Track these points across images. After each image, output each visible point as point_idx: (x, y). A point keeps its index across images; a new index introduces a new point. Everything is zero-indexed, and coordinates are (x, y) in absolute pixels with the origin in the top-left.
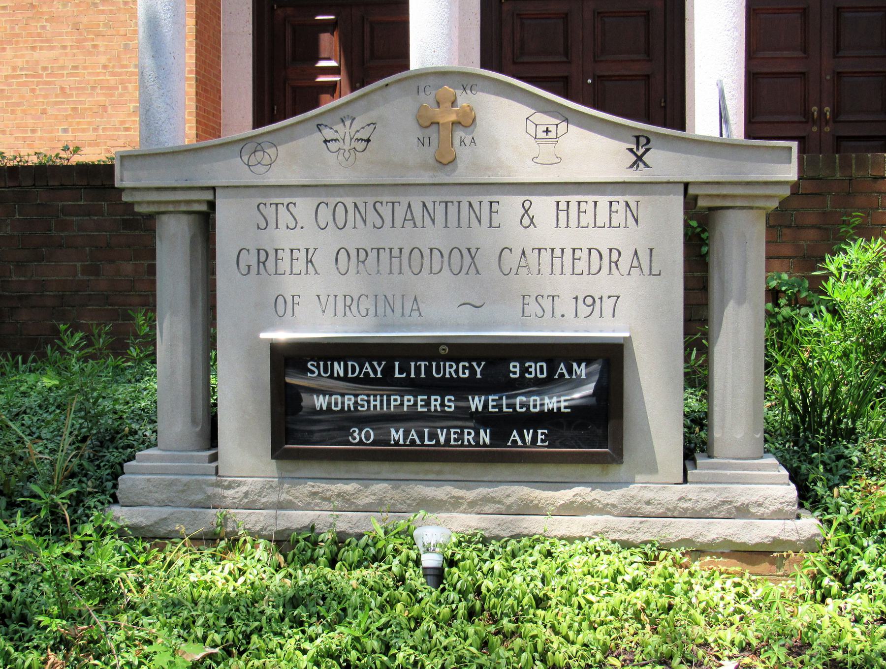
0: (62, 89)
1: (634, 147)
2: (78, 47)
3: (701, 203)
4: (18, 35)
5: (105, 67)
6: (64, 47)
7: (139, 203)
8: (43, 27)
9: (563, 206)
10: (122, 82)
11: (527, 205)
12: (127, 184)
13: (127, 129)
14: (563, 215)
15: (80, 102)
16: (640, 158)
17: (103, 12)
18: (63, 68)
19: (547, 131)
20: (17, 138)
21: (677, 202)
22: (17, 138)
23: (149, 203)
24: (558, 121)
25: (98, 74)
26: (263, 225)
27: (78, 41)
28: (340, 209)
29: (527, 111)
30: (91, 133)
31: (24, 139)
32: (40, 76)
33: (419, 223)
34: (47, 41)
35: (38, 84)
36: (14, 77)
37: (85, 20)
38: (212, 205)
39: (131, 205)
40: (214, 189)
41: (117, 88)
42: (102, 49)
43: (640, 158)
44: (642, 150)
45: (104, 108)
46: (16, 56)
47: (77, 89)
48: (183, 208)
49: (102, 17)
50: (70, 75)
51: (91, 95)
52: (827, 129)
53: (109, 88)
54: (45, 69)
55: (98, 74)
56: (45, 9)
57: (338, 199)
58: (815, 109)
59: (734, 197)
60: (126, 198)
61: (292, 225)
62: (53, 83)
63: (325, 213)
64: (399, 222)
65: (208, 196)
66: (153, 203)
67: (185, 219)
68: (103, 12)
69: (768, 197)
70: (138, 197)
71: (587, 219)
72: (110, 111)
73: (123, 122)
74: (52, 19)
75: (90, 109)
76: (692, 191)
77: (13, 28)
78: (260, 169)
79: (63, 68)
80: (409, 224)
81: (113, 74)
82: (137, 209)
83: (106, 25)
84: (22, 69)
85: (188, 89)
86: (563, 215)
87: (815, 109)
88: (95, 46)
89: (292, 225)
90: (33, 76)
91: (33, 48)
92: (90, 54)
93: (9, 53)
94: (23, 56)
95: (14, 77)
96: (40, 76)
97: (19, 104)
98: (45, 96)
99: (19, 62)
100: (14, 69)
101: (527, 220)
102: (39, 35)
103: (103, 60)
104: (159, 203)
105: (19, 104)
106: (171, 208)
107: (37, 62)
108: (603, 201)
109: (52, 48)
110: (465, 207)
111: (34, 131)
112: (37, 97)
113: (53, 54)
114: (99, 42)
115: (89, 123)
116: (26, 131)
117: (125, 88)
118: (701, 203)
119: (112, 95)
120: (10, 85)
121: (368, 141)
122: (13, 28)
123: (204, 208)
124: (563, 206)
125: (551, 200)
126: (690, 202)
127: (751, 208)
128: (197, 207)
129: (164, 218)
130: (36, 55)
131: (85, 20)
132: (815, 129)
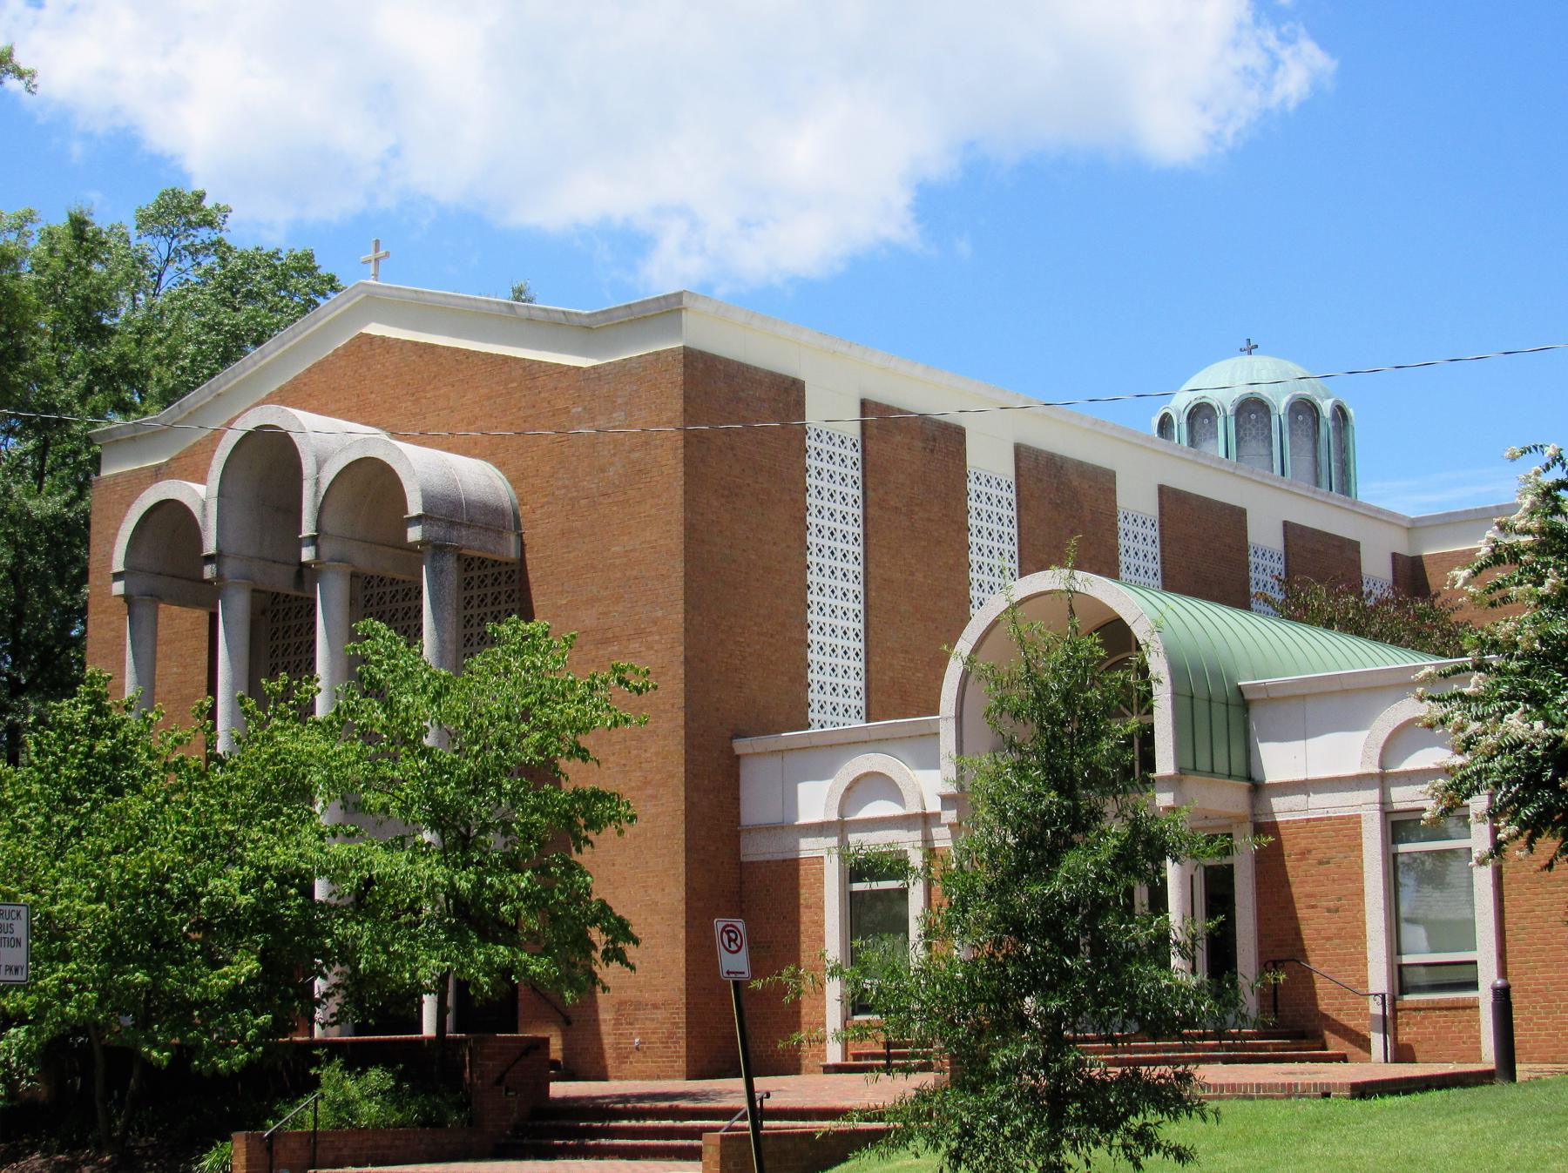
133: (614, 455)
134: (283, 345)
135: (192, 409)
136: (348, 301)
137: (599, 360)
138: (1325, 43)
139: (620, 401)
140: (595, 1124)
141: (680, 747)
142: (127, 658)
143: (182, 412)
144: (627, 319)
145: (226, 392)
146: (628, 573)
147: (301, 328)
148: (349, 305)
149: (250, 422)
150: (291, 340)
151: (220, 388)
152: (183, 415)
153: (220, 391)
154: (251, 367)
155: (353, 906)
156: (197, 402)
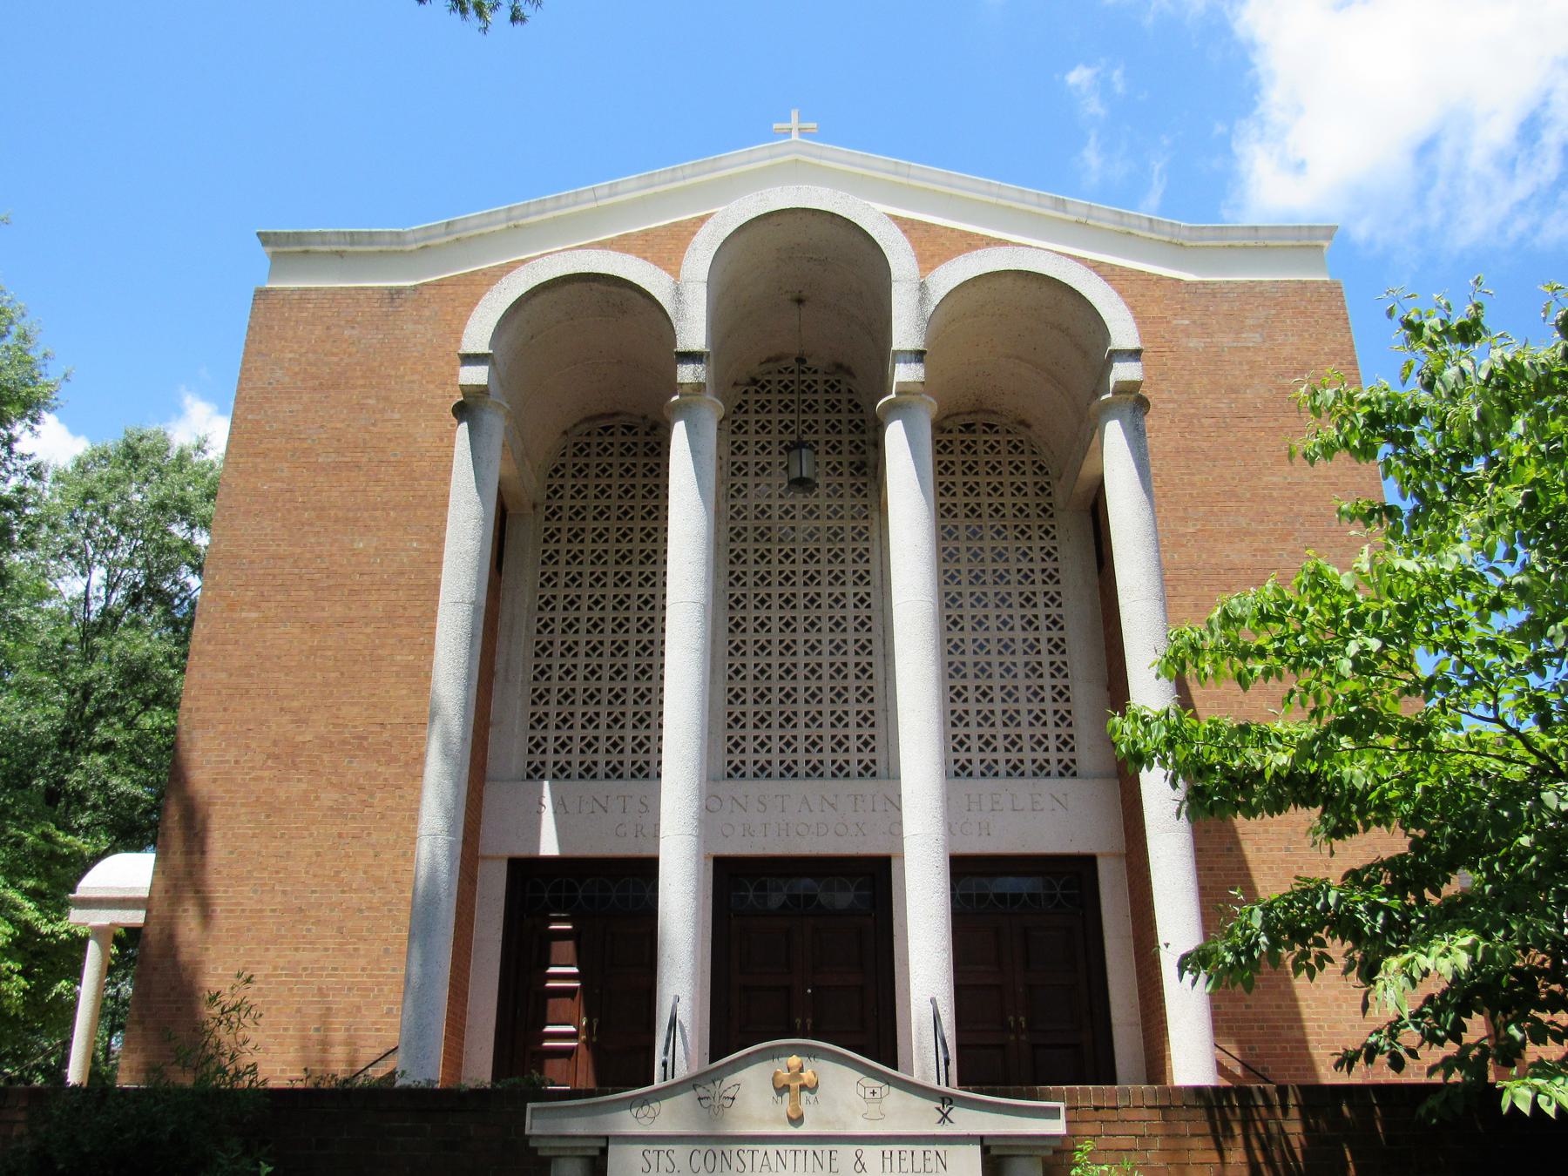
0: (320, 989)
1: (940, 1105)
2: (340, 950)
3: (994, 1152)
4: (283, 936)
5: (363, 969)
6: (326, 949)
7: (542, 1148)
8: (309, 930)
9: (887, 1155)
10: (379, 984)
11: (859, 1153)
12: (535, 1132)
13: (378, 1030)
14: (887, 1162)
15: (335, 1003)
16: (945, 1116)
17: (367, 918)
18: (322, 969)
19: (874, 1093)
20: (268, 1036)
21: (976, 1150)
22: (268, 1036)
23: (551, 1148)
24: (882, 1084)
25: (356, 976)
26: (647, 1169)
27: (341, 944)
28: (711, 1155)
29: (858, 1075)
30: (342, 1033)
31: (276, 1037)
32: (300, 976)
33: (774, 1168)
34: (310, 943)
35: (297, 982)
36: (273, 976)
37: (350, 924)
38: (604, 1152)
39: (536, 1149)
40: (607, 1138)
41: (373, 990)
42: (362, 952)
43: (945, 1116)
44: (947, 1109)
45: (359, 1008)
46: (279, 956)
47: (334, 989)
48: (579, 1153)
49: (366, 923)
50: (329, 976)
51: (347, 996)
52: (1023, 1037)
53: (366, 989)
54: (305, 969)
55: (356, 976)
56: (313, 913)
57: (709, 1147)
58: (1011, 1018)
59: (1018, 1147)
60: (532, 1144)
61: (670, 1169)
62: (312, 983)
63: (699, 1159)
64: (757, 1167)
65: (603, 1144)
66: (555, 1148)
67: (578, 1162)
68: (367, 918)
69: (1043, 1148)
70: (543, 1143)
71: (906, 1165)
72: (363, 1012)
73: (375, 1023)
74: (318, 922)
75: (345, 1009)
76: (987, 1142)
77: (279, 930)
78: (646, 1121)
79: (322, 969)
80: (765, 1169)
81: (370, 976)
82: (540, 1153)
83: (369, 930)
84: (282, 969)
85: (444, 993)
86: (887, 1162)
87: (1011, 1018)
88: (356, 950)
89: (670, 1169)
90: (294, 976)
91: (296, 949)
92: (351, 956)
93: (272, 954)
94: (285, 956)
95: (273, 976)
96: (300, 976)
97: (275, 1003)
98: (303, 996)
99: (281, 962)
100: (275, 968)
101: (859, 1167)
102: (304, 937)
103: (362, 962)
104: (560, 1148)
105: (275, 1003)
106: (569, 1153)
107: (299, 963)
108: (919, 1149)
109: (314, 950)
110: (810, 1154)
111: (286, 1030)
112: (294, 995)
113: (315, 955)
114: (361, 946)
115: (342, 1023)
116: (279, 1030)
117: (381, 990)
118: (994, 1152)
119: (368, 996)
120: (270, 983)
121: (733, 1099)
122: (279, 930)
123: (597, 1153)
124: (887, 1155)
125: (878, 1149)
126: (985, 1151)
127: (1031, 1156)
128: (591, 1153)
129: (561, 1161)
130: (299, 956)
131: (350, 924)
132: (1012, 1037)
133: (1251, 377)
134: (651, 186)
135: (465, 234)
136: (771, 157)
137: (1197, 274)
138: (74, 1086)
139: (1249, 322)
140: (1349, 1158)
141: (641, 1114)
142: (457, 449)
143: (448, 234)
144: (1242, 243)
145: (531, 226)
146: (1296, 508)
147: (688, 172)
148: (768, 163)
149: (872, 216)
150: (665, 183)
151: (527, 216)
152: (450, 238)
153: (522, 222)
154: (589, 201)
155: (108, 1076)
156: (477, 227)
